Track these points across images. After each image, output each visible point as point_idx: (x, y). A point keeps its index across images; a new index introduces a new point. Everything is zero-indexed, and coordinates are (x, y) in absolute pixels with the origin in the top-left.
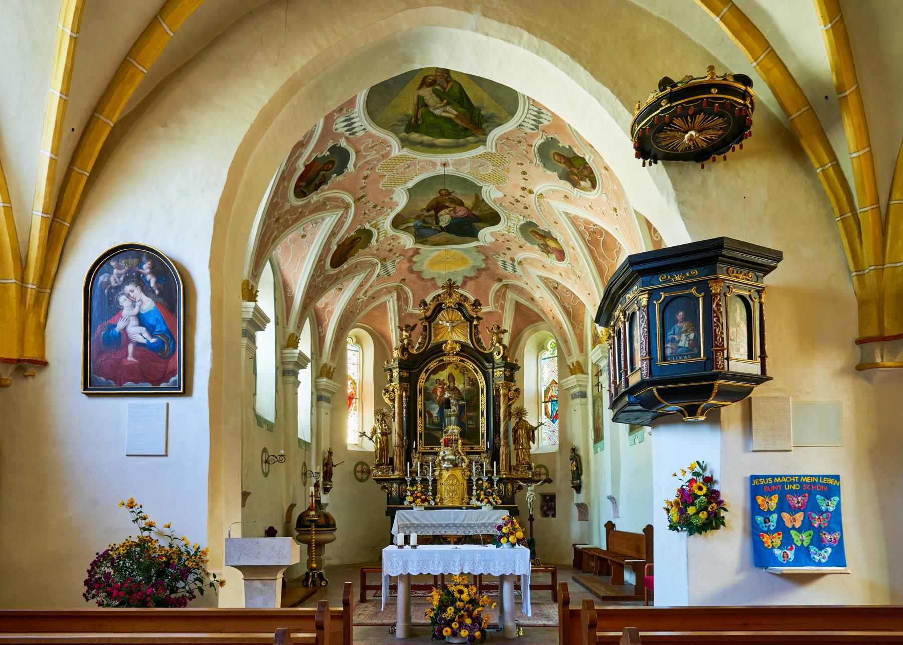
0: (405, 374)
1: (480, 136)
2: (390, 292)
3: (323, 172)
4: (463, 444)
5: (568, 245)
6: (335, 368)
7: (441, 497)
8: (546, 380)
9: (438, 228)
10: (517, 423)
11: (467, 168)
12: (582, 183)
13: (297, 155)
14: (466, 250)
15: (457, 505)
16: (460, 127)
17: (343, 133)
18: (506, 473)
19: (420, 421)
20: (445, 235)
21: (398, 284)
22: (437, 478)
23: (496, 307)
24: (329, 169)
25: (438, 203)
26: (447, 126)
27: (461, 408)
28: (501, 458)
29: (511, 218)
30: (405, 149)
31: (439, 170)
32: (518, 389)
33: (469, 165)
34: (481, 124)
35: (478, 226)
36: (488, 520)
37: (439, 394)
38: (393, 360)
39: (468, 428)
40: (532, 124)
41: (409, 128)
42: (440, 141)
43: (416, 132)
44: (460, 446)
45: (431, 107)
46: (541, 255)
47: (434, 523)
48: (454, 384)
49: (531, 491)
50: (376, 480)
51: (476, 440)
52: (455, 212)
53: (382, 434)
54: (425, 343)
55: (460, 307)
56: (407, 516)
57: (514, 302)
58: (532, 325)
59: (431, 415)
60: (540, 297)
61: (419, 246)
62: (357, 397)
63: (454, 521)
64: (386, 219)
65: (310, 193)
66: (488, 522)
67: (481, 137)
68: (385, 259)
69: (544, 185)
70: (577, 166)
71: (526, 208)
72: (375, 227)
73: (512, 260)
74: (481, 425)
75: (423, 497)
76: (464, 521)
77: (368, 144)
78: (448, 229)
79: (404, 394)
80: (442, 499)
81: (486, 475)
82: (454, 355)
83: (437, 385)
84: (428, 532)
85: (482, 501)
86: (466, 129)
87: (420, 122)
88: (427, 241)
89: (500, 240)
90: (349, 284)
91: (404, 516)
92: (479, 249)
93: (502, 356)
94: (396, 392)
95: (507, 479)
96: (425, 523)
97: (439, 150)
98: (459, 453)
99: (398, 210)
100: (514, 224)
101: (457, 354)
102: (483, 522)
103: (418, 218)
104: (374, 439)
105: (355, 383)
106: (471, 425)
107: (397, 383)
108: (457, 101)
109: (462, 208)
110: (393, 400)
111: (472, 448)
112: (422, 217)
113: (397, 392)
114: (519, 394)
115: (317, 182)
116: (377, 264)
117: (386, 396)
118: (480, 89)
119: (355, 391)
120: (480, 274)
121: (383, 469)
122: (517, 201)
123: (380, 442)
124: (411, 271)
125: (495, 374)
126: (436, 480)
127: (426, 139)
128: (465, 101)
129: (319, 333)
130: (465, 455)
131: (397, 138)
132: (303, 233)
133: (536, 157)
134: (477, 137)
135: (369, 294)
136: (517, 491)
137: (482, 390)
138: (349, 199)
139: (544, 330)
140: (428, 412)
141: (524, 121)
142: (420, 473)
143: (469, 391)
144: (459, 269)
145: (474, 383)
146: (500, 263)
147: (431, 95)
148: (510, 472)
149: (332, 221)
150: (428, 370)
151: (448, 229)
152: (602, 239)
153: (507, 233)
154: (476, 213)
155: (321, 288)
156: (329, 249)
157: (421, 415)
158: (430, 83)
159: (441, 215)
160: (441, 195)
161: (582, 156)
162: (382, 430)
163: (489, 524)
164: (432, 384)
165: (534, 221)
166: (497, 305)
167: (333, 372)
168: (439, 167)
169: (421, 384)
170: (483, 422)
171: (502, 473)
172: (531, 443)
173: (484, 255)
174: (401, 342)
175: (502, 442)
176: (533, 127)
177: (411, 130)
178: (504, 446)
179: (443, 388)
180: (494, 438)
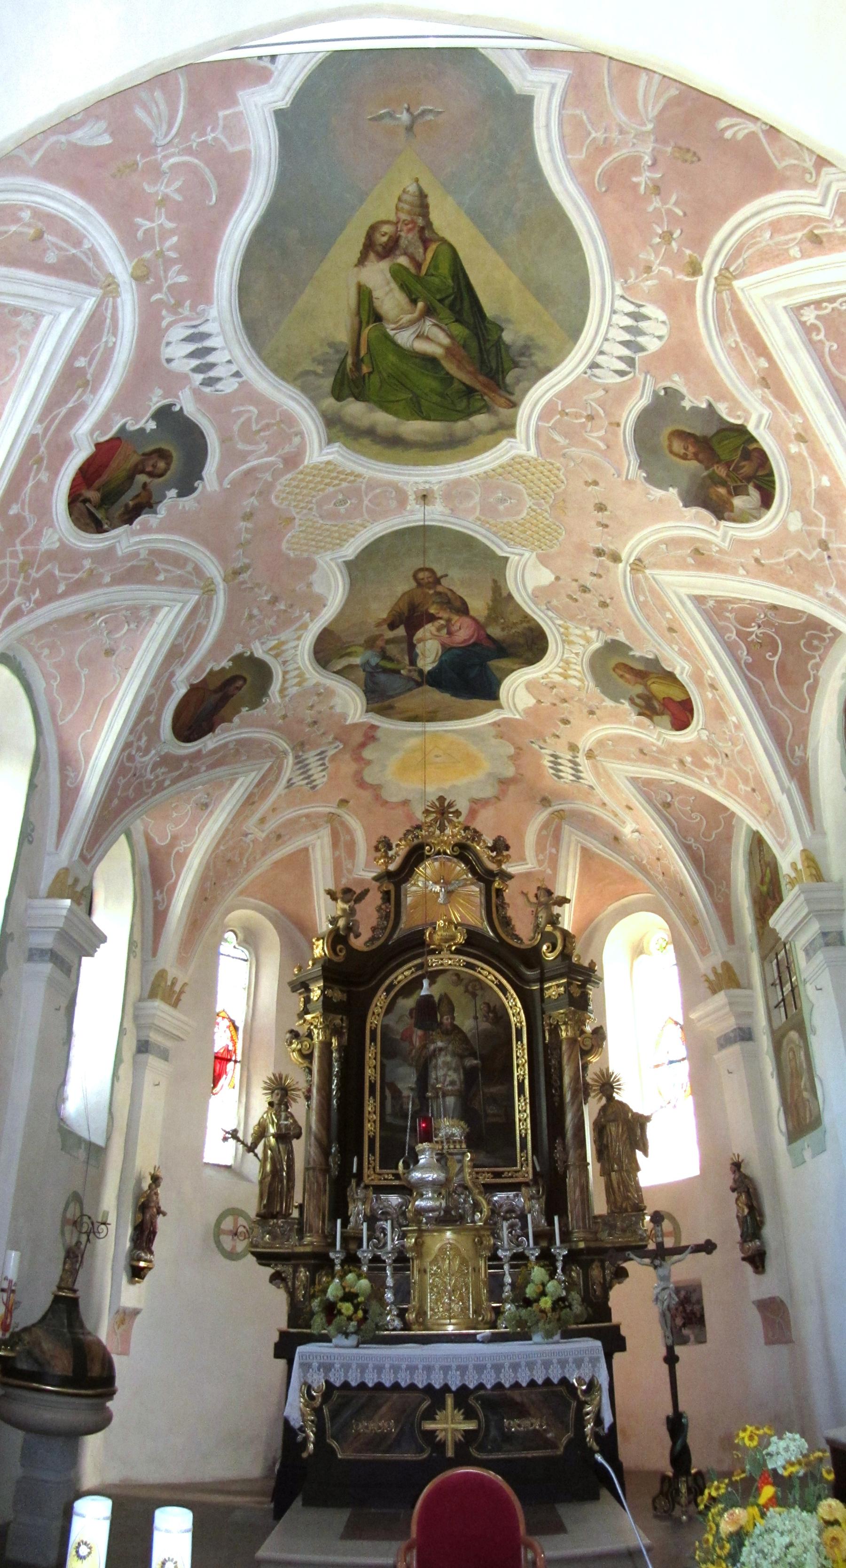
0: (337, 995)
1: (501, 410)
2: (315, 827)
3: (141, 478)
5: (698, 677)
6: (185, 984)
9: (415, 676)
11: (474, 508)
12: (738, 502)
13: (70, 405)
14: (474, 735)
16: (456, 385)
17: (185, 377)
19: (370, 1106)
20: (434, 696)
21: (333, 810)
22: (409, 1255)
23: (540, 863)
24: (157, 471)
25: (413, 607)
26: (428, 383)
27: (470, 1076)
29: (572, 638)
30: (336, 447)
31: (412, 512)
33: (477, 498)
34: (504, 373)
35: (498, 668)
38: (310, 963)
40: (620, 358)
41: (342, 384)
42: (414, 428)
43: (357, 398)
44: (467, 1170)
45: (389, 322)
46: (637, 724)
48: (453, 1018)
52: (450, 633)
53: (279, 1137)
54: (385, 928)
55: (463, 852)
59: (397, 1094)
60: (633, 832)
61: (375, 719)
62: (239, 1058)
64: (299, 638)
65: (113, 527)
67: (504, 412)
68: (302, 744)
69: (608, 726)
70: (725, 456)
71: (604, 605)
72: (276, 656)
73: (573, 748)
77: (249, 419)
78: (435, 679)
79: (335, 1042)
81: (536, 1243)
82: (452, 953)
86: (469, 391)
87: (365, 369)
88: (391, 707)
89: (547, 702)
90: (224, 794)
92: (503, 729)
93: (562, 953)
94: (315, 1036)
95: (588, 1251)
97: (412, 453)
99: (327, 615)
100: (577, 654)
101: (458, 952)
103: (370, 643)
104: (259, 1150)
106: (494, 1115)
107: (317, 1014)
108: (447, 302)
109: (466, 621)
110: (308, 1057)
111: (498, 1175)
112: (380, 643)
113: (318, 1036)
115: (128, 499)
116: (285, 753)
117: (294, 1046)
118: (500, 261)
119: (234, 1045)
120: (504, 792)
122: (585, 589)
123: (272, 1158)
124: (362, 784)
125: (547, 994)
126: (407, 1260)
127: (383, 419)
128: (466, 304)
129: (156, 904)
130: (480, 1193)
131: (315, 413)
132: (107, 643)
133: (628, 454)
134: (495, 413)
135: (272, 824)
137: (519, 1032)
138: (213, 570)
140: (388, 1085)
141: (601, 353)
142: (369, 1240)
144: (462, 781)
145: (500, 1016)
146: (546, 762)
147: (388, 283)
149: (172, 616)
151: (435, 679)
152: (776, 659)
153: (561, 679)
154: (495, 631)
155: (149, 783)
156: (168, 691)
157: (372, 1093)
158: (385, 246)
159: (421, 640)
160: (419, 584)
161: (739, 422)
162: (279, 1126)
165: (621, 637)
166: (541, 857)
167: (181, 992)
168: (412, 504)
169: (374, 1020)
170: (522, 1109)
173: (513, 744)
174: (331, 923)
176: (622, 366)
177: (346, 391)
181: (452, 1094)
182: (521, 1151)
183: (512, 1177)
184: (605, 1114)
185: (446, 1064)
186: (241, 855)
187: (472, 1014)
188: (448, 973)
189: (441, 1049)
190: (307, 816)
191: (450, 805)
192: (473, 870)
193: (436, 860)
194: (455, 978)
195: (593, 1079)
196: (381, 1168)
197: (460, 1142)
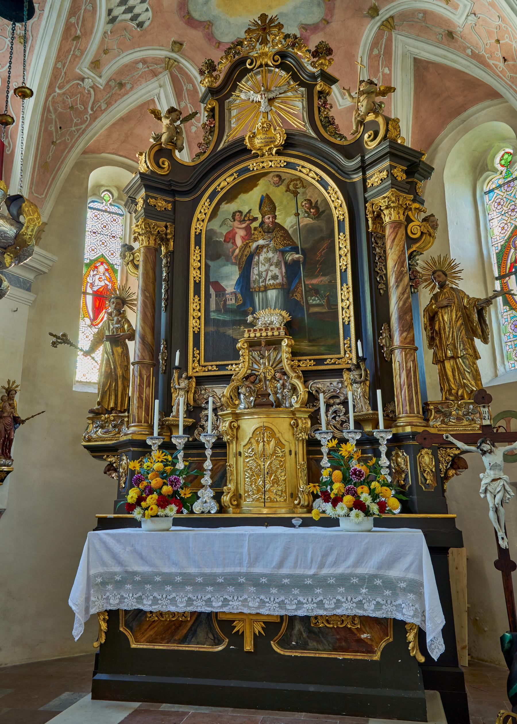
2: (155, 74)
4: (294, 354)
7: (237, 489)
8: (497, 231)
10: (435, 297)
15: (283, 513)
18: (415, 420)
28: (397, 381)
32: (432, 215)
36: (357, 564)
37: (239, 242)
39: (310, 315)
47: (192, 570)
48: (275, 217)
49: (494, 467)
50: (92, 449)
51: (330, 342)
56: (117, 548)
57: (410, 63)
58: (455, 121)
59: (220, 291)
63: (251, 564)
66: (360, 571)
74: (340, 305)
75: (167, 489)
76: (281, 565)
80: (237, 497)
83: (236, 224)
84: (173, 601)
85: (336, 501)
91: (108, 549)
96: (166, 570)
98: (285, 374)
101: (278, 153)
102: (340, 570)
105: (115, 271)
114: (435, 227)
121: (107, 421)
125: (369, 182)
130: (298, 377)
136: (451, 472)
137: (341, 223)
139: (484, 122)
143: (310, 230)
148: (427, 420)
150: (215, 193)
157: (197, 292)
163: (362, 578)
164: (223, 223)
169: (196, 227)
171: (401, 422)
172: (477, 342)
175: (397, 340)
178: (403, 348)
179: (248, 229)
180: (377, 333)
181: (274, 287)
182: (344, 339)
183: (334, 364)
184: (436, 301)
185: (268, 260)
186: (84, 103)
187: (294, 211)
188: (271, 175)
189: (263, 247)
190: (144, 61)
191: (272, 20)
192: (295, 77)
193: (258, 73)
194: (276, 179)
195: (423, 268)
196: (205, 361)
197: (278, 329)
